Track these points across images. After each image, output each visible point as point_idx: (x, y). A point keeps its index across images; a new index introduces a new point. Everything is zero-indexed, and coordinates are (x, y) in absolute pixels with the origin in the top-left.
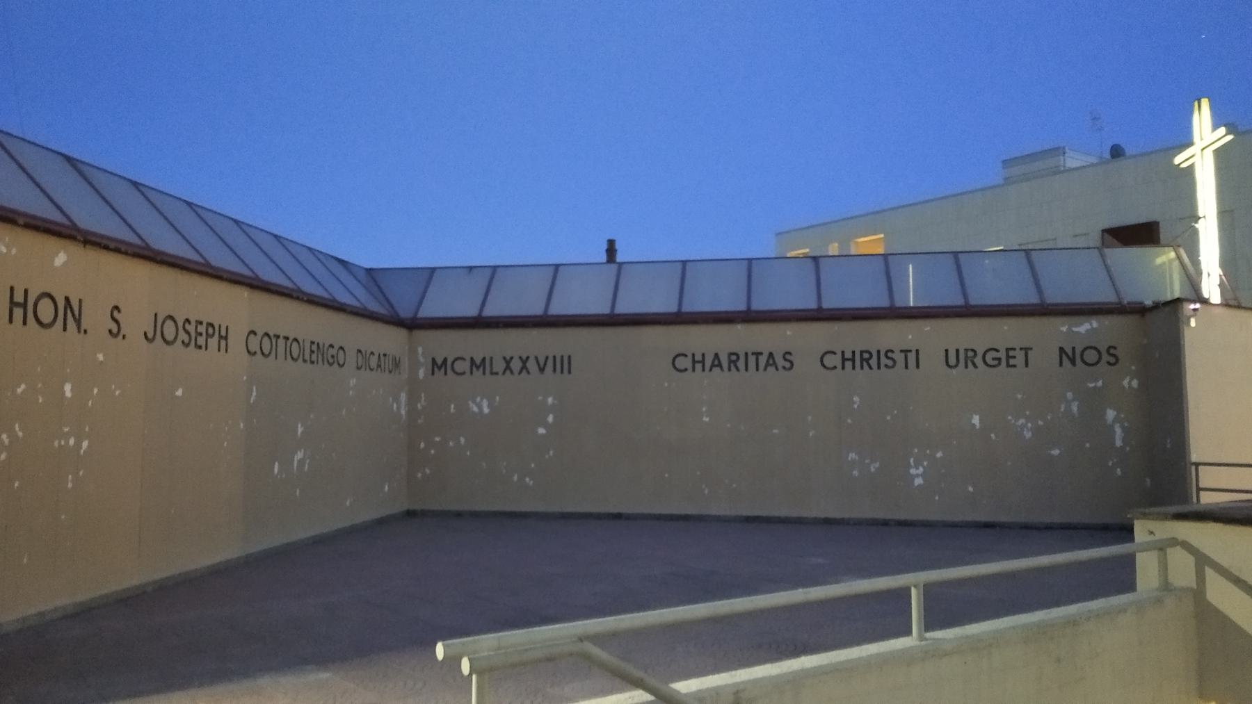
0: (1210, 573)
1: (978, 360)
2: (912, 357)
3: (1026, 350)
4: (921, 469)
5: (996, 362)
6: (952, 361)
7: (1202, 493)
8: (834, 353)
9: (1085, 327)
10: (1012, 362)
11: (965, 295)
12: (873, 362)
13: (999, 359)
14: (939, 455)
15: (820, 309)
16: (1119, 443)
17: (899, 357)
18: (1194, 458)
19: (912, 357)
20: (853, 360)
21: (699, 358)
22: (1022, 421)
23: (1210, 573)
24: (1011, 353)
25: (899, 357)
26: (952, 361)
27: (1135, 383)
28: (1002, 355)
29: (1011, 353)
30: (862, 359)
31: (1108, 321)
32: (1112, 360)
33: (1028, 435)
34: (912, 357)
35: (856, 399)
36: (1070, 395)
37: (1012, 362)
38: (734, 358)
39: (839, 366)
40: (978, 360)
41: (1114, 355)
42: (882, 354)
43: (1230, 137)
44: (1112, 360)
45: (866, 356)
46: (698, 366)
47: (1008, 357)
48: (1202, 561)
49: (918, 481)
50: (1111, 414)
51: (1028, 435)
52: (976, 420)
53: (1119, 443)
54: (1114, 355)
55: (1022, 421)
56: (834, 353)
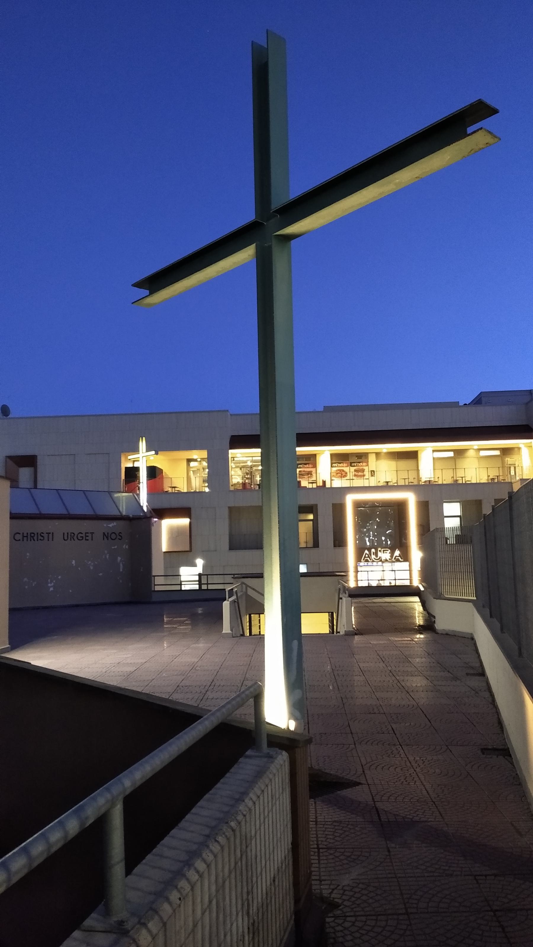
0: (248, 588)
1: (75, 538)
2: (51, 535)
3: (92, 533)
4: (53, 584)
5: (81, 538)
6: (66, 538)
7: (156, 586)
8: (19, 534)
9: (112, 524)
10: (87, 538)
11: (38, 509)
12: (35, 538)
13: (82, 537)
14: (60, 577)
15: (40, 514)
16: (121, 570)
17: (46, 536)
18: (154, 574)
19: (51, 535)
20: (27, 537)
21: (25, 535)
22: (90, 562)
23: (248, 588)
24: (87, 535)
25: (46, 536)
26: (66, 538)
27: (127, 547)
28: (84, 535)
29: (87, 535)
30: (31, 536)
31: (121, 523)
32: (120, 538)
33: (92, 568)
34: (50, 535)
35: (28, 554)
36: (106, 552)
37: (87, 538)
38: (33, 535)
39: (21, 540)
40: (75, 538)
41: (42, 536)
42: (39, 535)
43: (144, 438)
44: (120, 538)
45: (33, 535)
46: (25, 538)
47: (86, 536)
48: (247, 586)
49: (51, 589)
50: (119, 558)
51: (92, 568)
52: (74, 562)
53: (121, 570)
54: (42, 536)
55: (90, 562)
56: (19, 534)
